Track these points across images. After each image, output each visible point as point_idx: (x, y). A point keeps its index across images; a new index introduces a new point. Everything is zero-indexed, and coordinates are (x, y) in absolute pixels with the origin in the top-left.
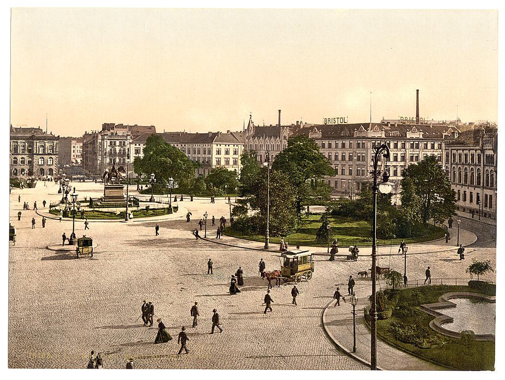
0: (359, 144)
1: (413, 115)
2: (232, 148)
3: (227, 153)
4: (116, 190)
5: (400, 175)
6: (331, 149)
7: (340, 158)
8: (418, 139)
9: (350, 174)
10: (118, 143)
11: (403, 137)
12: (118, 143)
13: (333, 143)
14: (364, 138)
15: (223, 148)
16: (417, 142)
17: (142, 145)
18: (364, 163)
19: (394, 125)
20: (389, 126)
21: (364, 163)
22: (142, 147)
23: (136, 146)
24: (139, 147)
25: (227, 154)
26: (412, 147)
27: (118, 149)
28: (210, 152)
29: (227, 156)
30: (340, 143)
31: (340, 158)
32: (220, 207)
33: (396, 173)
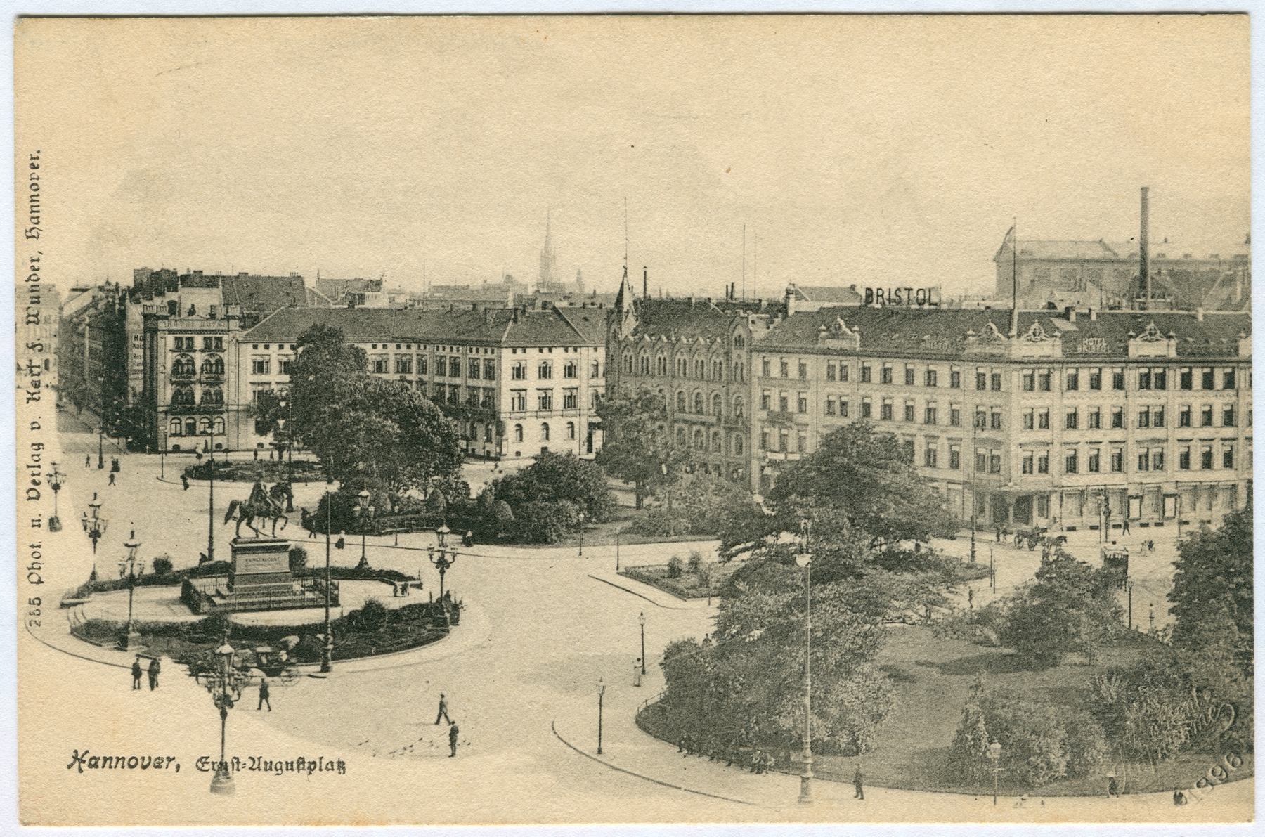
0: (980, 376)
1: (988, 564)
2: (558, 359)
3: (545, 372)
4: (267, 556)
5: (1200, 387)
6: (891, 388)
7: (920, 415)
8: (1164, 361)
9: (955, 464)
10: (199, 342)
11: (1120, 356)
12: (199, 342)
13: (898, 368)
14: (993, 358)
15: (533, 359)
16: (1160, 371)
17: (274, 347)
18: (998, 435)
19: (1088, 316)
20: (1073, 317)
21: (998, 435)
22: (276, 355)
23: (256, 352)
24: (267, 352)
25: (545, 376)
26: (1145, 383)
27: (199, 359)
28: (491, 373)
29: (545, 383)
30: (920, 369)
31: (920, 415)
32: (242, 491)
33: (1190, 380)
